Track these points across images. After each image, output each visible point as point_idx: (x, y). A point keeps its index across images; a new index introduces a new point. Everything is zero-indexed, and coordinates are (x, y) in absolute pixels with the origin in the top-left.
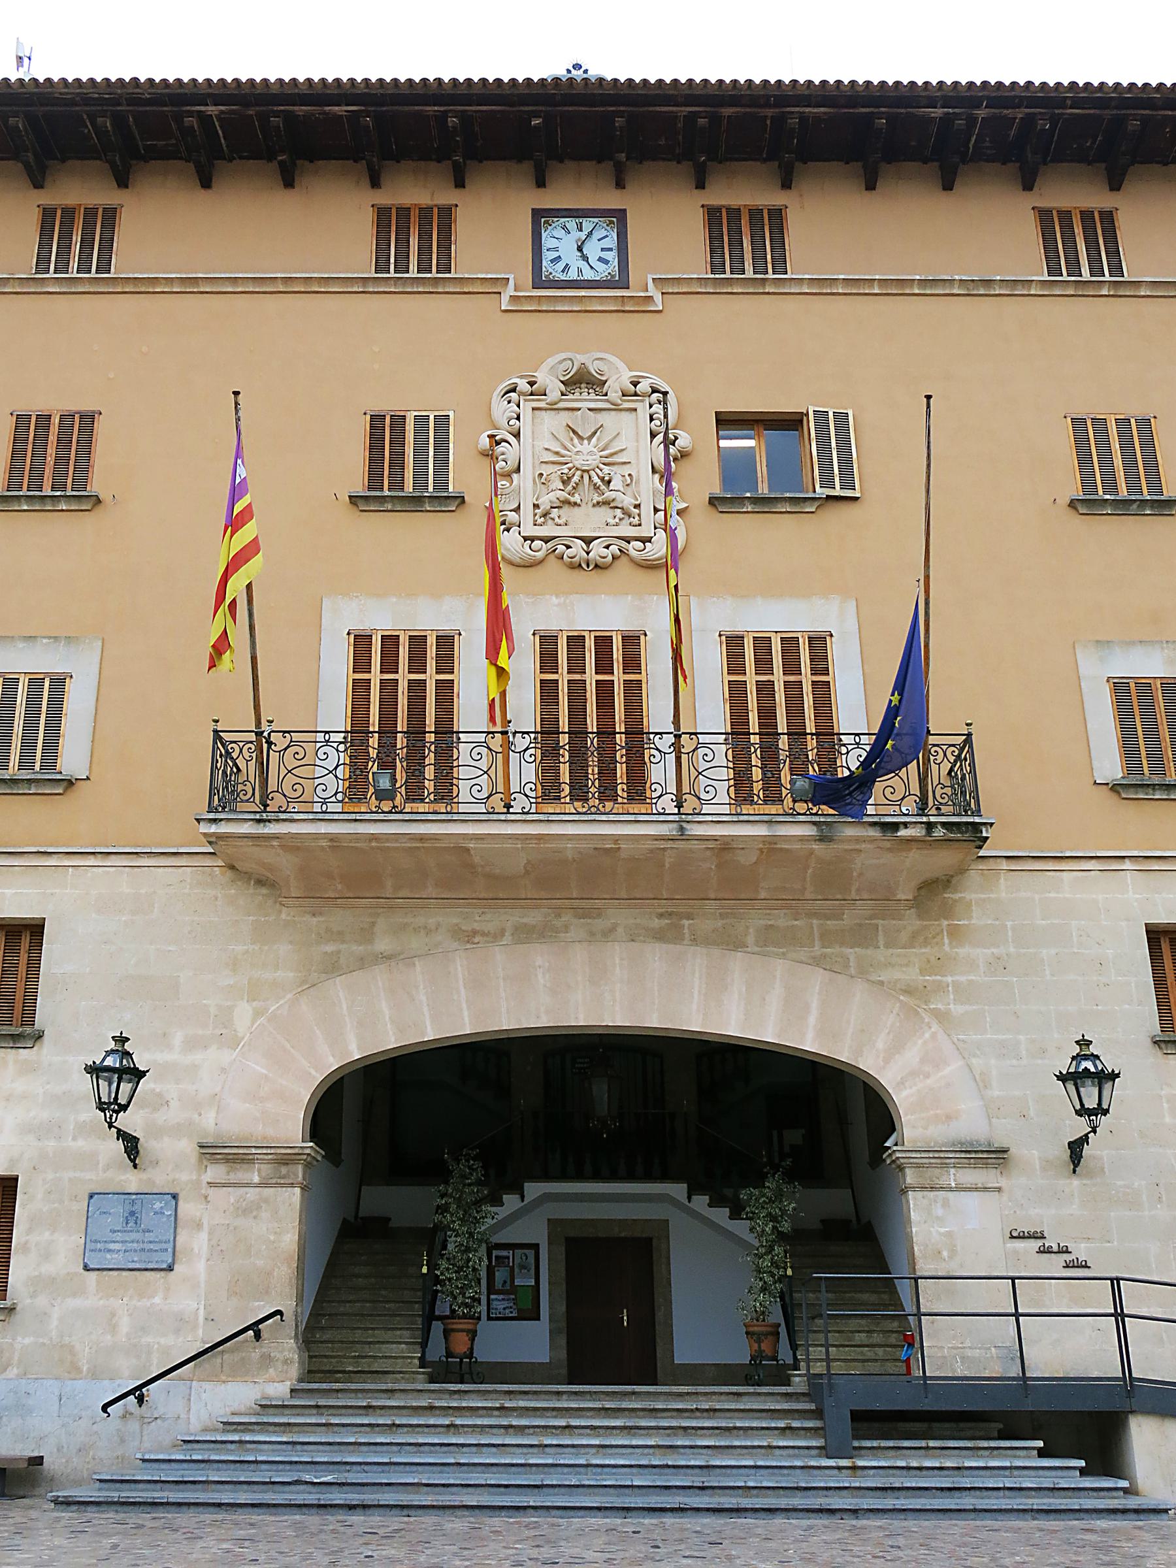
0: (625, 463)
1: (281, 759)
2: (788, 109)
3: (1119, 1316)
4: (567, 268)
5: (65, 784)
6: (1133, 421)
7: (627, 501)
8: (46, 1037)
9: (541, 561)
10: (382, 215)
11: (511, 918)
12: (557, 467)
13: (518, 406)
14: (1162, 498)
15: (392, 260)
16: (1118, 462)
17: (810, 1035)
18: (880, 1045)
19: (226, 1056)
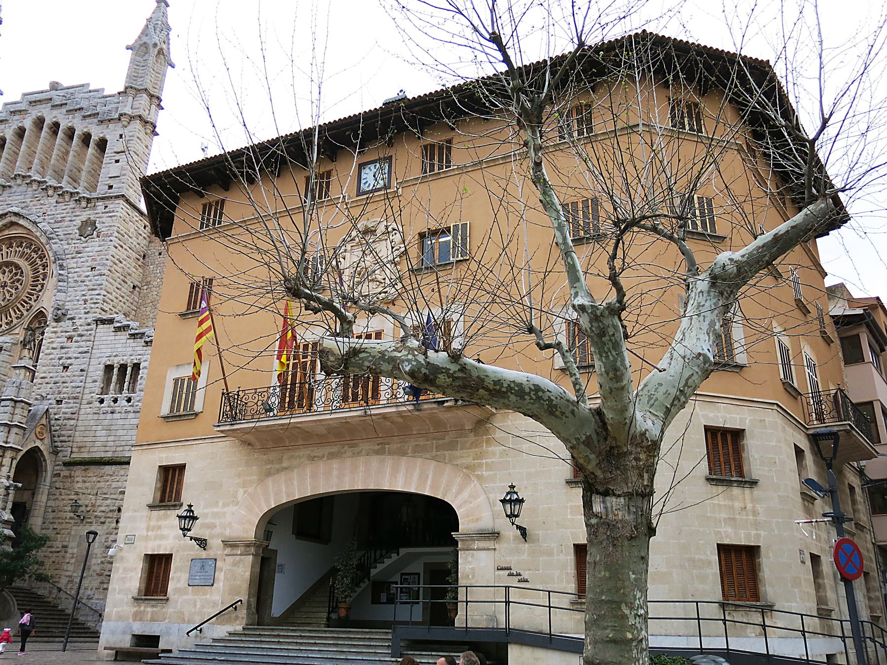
3: (507, 602)
11: (327, 450)
17: (428, 488)
18: (454, 491)
19: (235, 508)
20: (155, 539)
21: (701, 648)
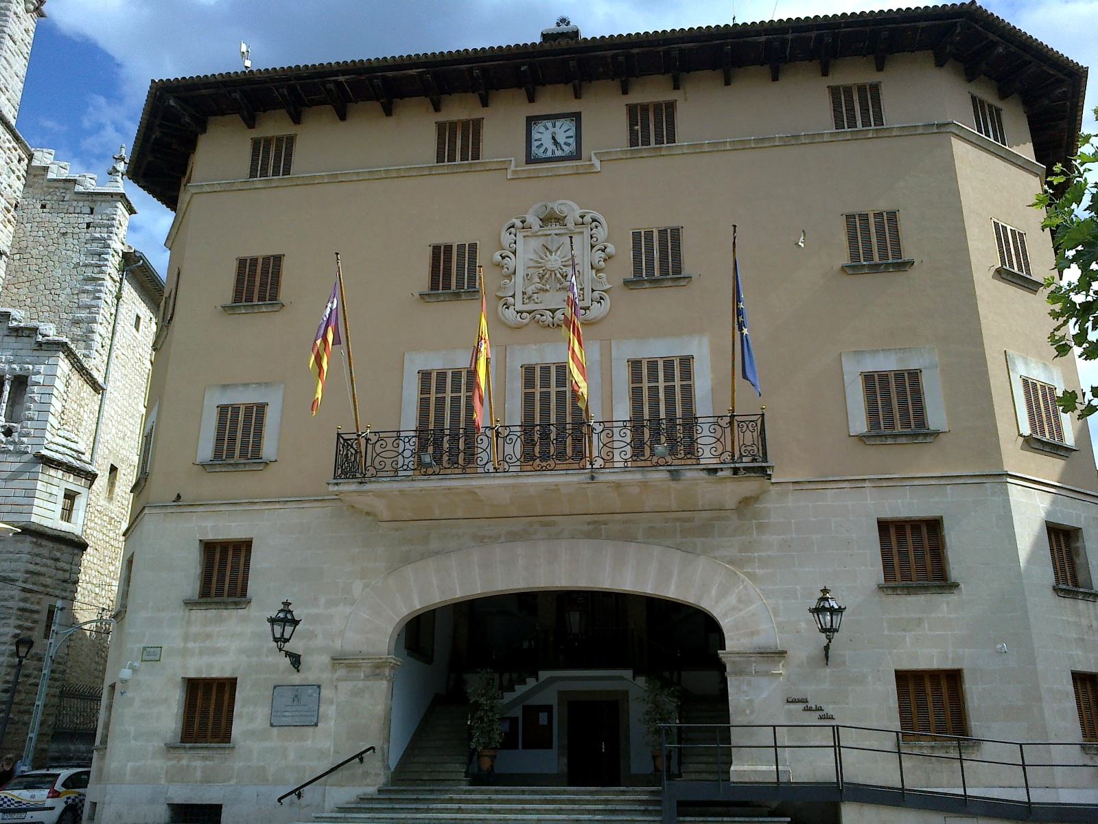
1: (374, 448)
2: (672, 46)
4: (546, 150)
5: (264, 464)
6: (885, 214)
8: (252, 603)
9: (527, 324)
10: (632, 110)
13: (515, 236)
14: (654, 278)
15: (446, 154)
16: (874, 240)
17: (673, 587)
18: (713, 592)
19: (348, 610)
21: (1029, 802)
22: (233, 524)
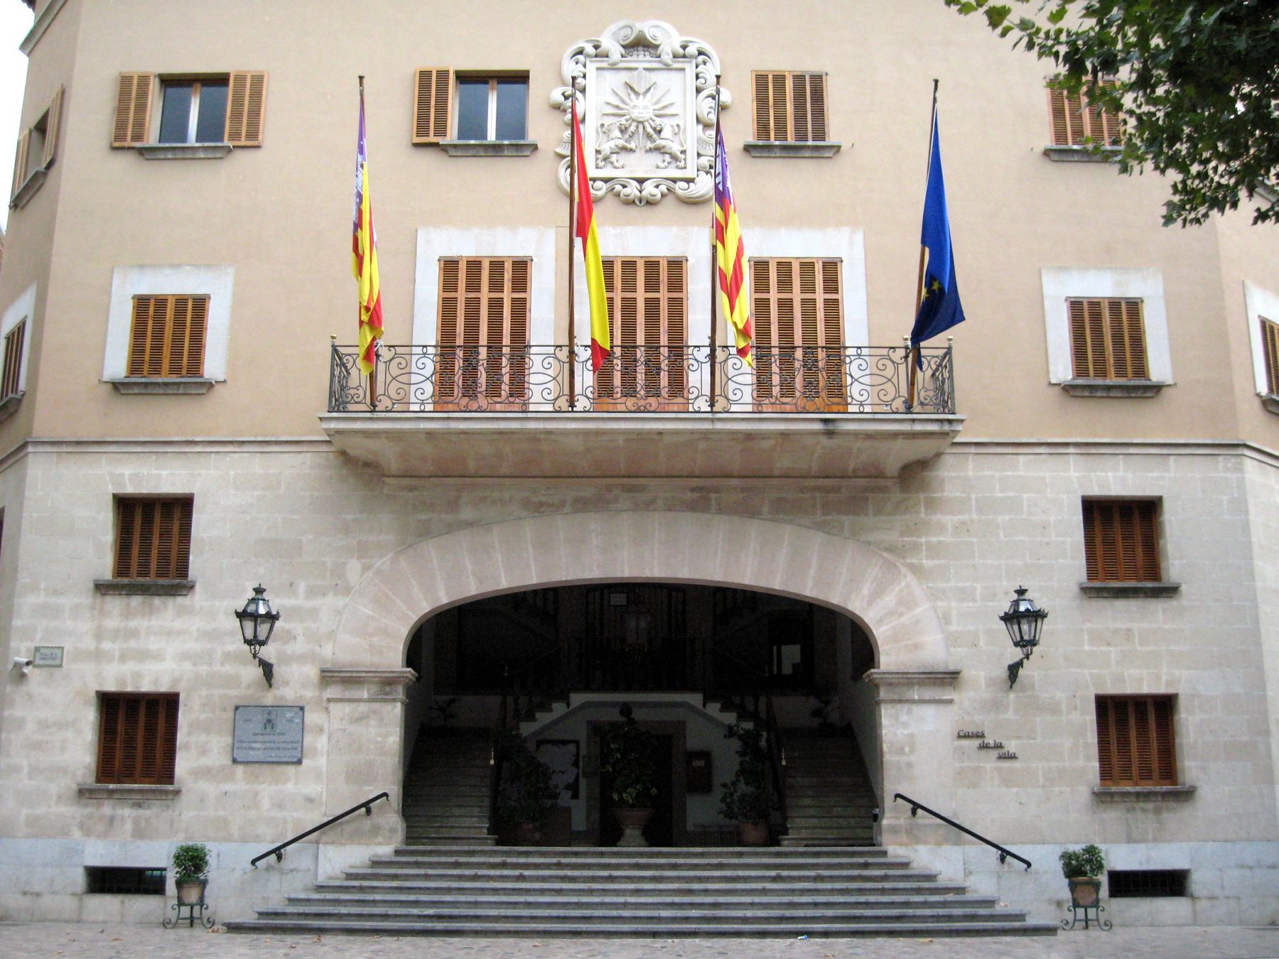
0: (673, 115)
7: (676, 148)
12: (617, 119)
13: (585, 66)
17: (810, 584)
18: (865, 592)
19: (341, 602)
20: (123, 657)
22: (164, 473)
